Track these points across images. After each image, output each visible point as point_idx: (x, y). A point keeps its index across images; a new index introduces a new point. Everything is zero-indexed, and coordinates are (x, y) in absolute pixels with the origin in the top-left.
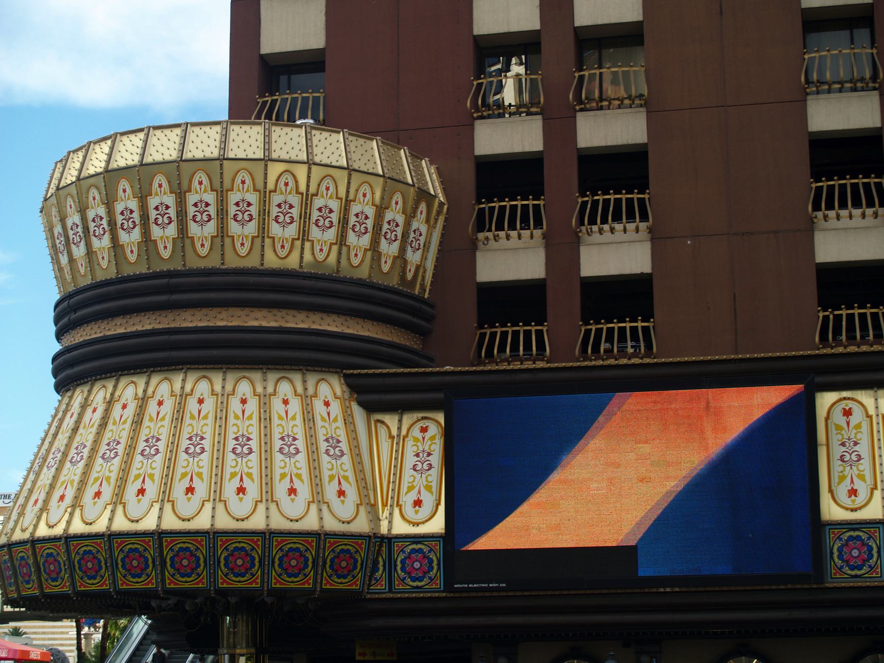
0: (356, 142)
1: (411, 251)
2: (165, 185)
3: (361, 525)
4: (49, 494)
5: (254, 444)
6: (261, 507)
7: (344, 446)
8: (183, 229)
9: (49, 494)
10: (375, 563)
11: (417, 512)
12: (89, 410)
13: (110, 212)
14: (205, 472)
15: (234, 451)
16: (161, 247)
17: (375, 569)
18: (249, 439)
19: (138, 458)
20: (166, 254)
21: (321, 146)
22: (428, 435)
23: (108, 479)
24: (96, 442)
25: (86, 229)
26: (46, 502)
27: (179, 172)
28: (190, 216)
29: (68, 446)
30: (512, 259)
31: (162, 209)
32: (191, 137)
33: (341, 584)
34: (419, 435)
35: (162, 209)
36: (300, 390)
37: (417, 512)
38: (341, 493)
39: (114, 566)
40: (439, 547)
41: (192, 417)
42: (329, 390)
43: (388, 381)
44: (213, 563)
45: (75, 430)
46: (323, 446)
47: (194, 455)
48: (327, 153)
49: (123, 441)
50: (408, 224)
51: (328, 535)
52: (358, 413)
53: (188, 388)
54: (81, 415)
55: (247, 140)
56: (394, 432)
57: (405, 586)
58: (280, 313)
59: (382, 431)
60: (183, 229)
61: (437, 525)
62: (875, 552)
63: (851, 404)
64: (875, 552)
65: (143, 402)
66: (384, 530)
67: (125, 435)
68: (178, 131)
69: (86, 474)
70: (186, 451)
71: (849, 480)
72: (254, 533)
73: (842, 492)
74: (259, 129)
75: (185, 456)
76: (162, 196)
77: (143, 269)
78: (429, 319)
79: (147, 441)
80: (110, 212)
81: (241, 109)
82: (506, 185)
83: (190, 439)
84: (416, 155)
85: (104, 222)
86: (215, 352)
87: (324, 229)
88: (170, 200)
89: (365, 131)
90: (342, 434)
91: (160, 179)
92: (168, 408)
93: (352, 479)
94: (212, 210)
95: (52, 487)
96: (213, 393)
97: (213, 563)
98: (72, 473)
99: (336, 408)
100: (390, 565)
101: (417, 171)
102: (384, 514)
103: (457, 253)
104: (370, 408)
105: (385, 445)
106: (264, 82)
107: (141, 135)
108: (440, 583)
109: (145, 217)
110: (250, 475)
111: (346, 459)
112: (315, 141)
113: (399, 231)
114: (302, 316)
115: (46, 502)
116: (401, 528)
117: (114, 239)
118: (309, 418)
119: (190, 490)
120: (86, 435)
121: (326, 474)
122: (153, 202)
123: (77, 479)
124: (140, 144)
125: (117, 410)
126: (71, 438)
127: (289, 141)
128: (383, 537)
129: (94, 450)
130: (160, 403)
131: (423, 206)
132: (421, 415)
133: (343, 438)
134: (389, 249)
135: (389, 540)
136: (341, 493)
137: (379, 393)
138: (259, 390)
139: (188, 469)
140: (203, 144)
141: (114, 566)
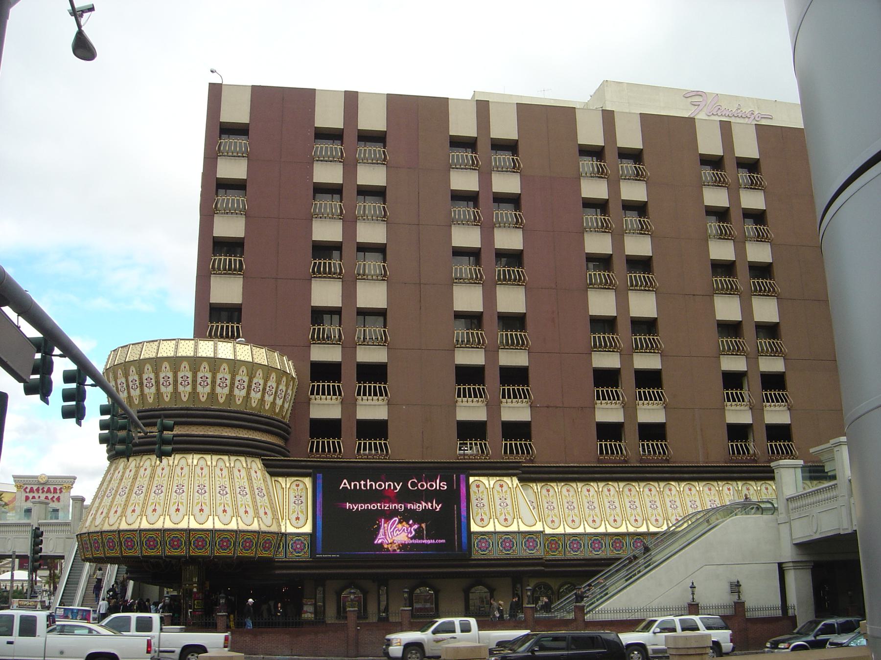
0: (255, 350)
1: (276, 399)
2: (187, 367)
3: (274, 529)
4: (97, 511)
5: (228, 490)
6: (234, 519)
7: (247, 490)
9: (97, 511)
10: (279, 544)
12: (128, 471)
13: (141, 379)
14: (230, 502)
16: (183, 396)
17: (279, 547)
20: (238, 403)
21: (241, 351)
25: (128, 386)
26: (108, 513)
27: (175, 362)
29: (106, 489)
30: (326, 408)
31: (185, 378)
32: (180, 345)
33: (266, 554)
36: (245, 465)
38: (246, 512)
39: (104, 546)
40: (309, 539)
42: (257, 465)
43: (274, 463)
44: (213, 544)
45: (110, 481)
46: (257, 492)
47: (138, 495)
48: (225, 352)
50: (277, 387)
51: (217, 531)
52: (267, 475)
53: (176, 462)
54: (124, 473)
55: (206, 348)
56: (284, 486)
57: (293, 556)
58: (237, 430)
59: (278, 485)
61: (308, 528)
65: (138, 468)
66: (283, 531)
67: (146, 483)
68: (174, 342)
69: (112, 502)
72: (207, 530)
73: (478, 519)
74: (212, 343)
76: (148, 374)
77: (242, 409)
78: (289, 433)
80: (141, 379)
81: (200, 333)
82: (325, 373)
84: (282, 354)
85: (137, 383)
87: (166, 387)
89: (260, 344)
90: (246, 485)
92: (148, 472)
93: (251, 506)
94: (209, 381)
95: (98, 508)
96: (169, 465)
97: (213, 544)
98: (120, 500)
99: (259, 473)
100: (286, 546)
101: (282, 362)
102: (283, 524)
103: (301, 404)
104: (272, 474)
105: (280, 491)
106: (215, 319)
107: (156, 343)
108: (308, 554)
110: (228, 504)
111: (248, 496)
112: (238, 349)
113: (274, 390)
114: (245, 432)
115: (108, 513)
116: (291, 529)
117: (142, 391)
118: (250, 479)
119: (155, 510)
120: (127, 482)
121: (239, 503)
122: (180, 374)
123: (123, 503)
124: (156, 347)
125: (142, 471)
126: (108, 485)
127: (225, 350)
128: (283, 534)
129: (131, 490)
130: (163, 469)
131: (284, 379)
132: (498, 478)
133: (247, 487)
134: (269, 399)
135: (285, 535)
136: (246, 512)
137: (278, 466)
138: (228, 465)
140: (186, 350)
141: (104, 546)
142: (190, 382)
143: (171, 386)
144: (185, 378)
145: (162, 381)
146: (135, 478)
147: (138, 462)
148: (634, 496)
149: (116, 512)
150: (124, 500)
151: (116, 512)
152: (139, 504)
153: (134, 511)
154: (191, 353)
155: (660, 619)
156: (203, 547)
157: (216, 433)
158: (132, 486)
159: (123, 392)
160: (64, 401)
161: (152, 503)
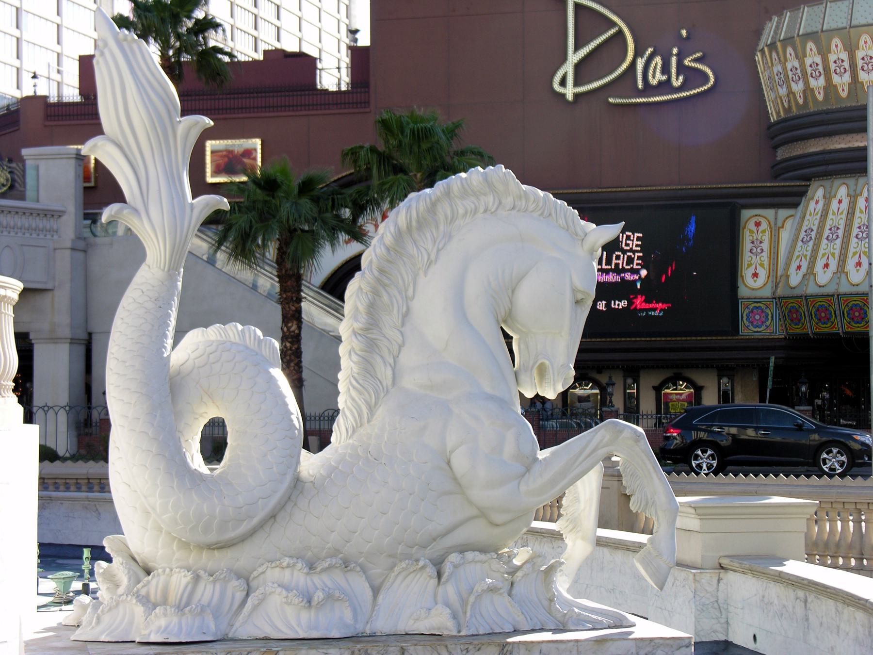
8: (828, 79)
11: (755, 281)
13: (825, 61)
15: (857, 237)
18: (838, 228)
19: (824, 241)
22: (761, 228)
23: (833, 255)
24: (821, 227)
28: (832, 70)
31: (867, 60)
34: (754, 228)
35: (814, 66)
37: (755, 281)
41: (834, 214)
49: (842, 227)
60: (828, 79)
62: (770, 317)
63: (760, 219)
64: (770, 317)
70: (857, 237)
71: (753, 267)
75: (855, 240)
79: (830, 229)
80: (825, 61)
83: (859, 228)
86: (848, 165)
88: (844, 56)
91: (836, 41)
109: (826, 68)
125: (834, 204)
130: (840, 202)
139: (826, 251)
142: (848, 68)
143: (822, 77)
144: (814, 66)
145: (833, 66)
146: (851, 213)
147: (852, 187)
148: (764, 231)
149: (799, 267)
150: (810, 248)
151: (799, 267)
152: (805, 256)
153: (826, 266)
154: (843, 22)
155: (344, 329)
156: (851, 309)
157: (843, 146)
158: (821, 227)
159: (781, 86)
160: (85, 182)
161: (823, 255)
